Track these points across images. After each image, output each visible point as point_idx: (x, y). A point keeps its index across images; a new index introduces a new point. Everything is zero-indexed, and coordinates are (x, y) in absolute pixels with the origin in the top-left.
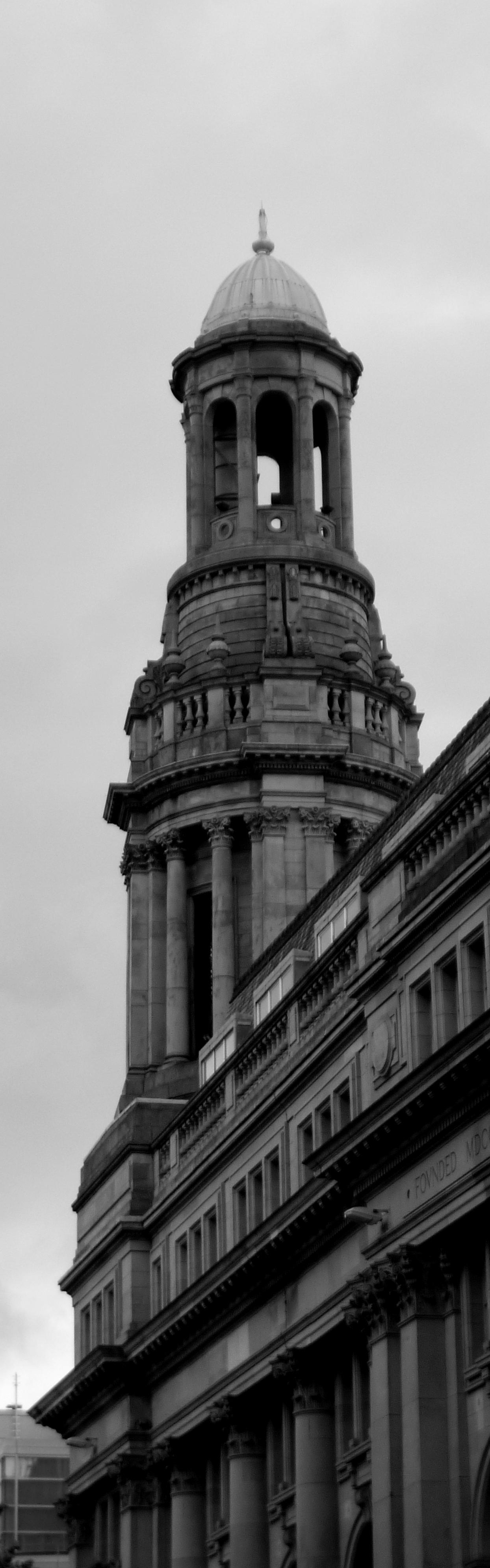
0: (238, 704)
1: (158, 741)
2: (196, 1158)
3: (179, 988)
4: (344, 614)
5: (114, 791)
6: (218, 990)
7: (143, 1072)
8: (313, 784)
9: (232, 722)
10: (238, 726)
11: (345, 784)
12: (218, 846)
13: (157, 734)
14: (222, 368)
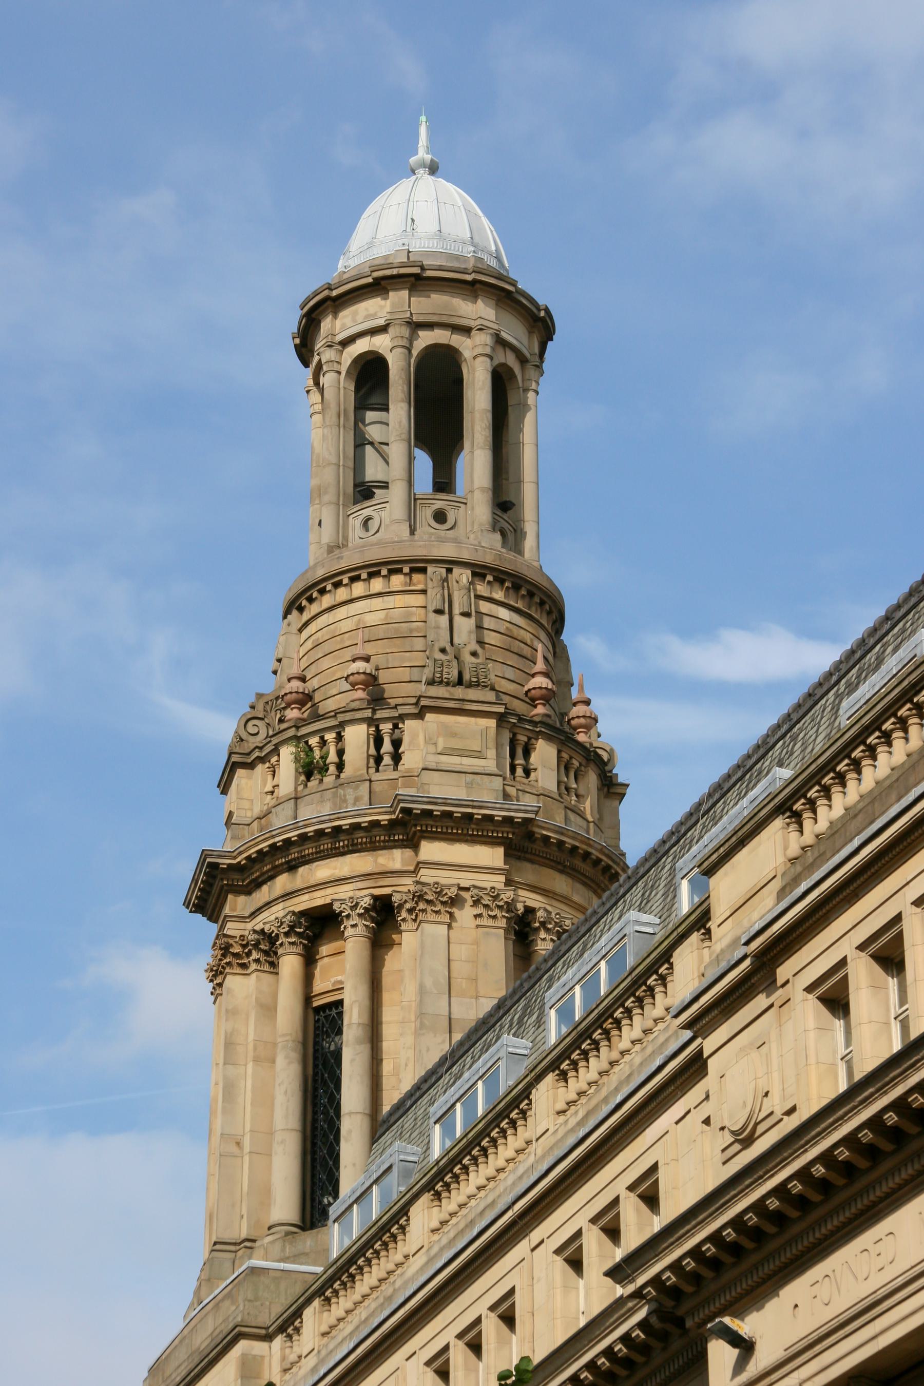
0: (387, 746)
1: (269, 797)
2: (351, 1334)
3: (297, 1131)
4: (529, 643)
5: (208, 860)
6: (350, 1132)
7: (232, 1248)
8: (493, 856)
9: (377, 770)
10: (387, 772)
11: (532, 862)
12: (355, 936)
13: (269, 788)
14: (372, 311)
